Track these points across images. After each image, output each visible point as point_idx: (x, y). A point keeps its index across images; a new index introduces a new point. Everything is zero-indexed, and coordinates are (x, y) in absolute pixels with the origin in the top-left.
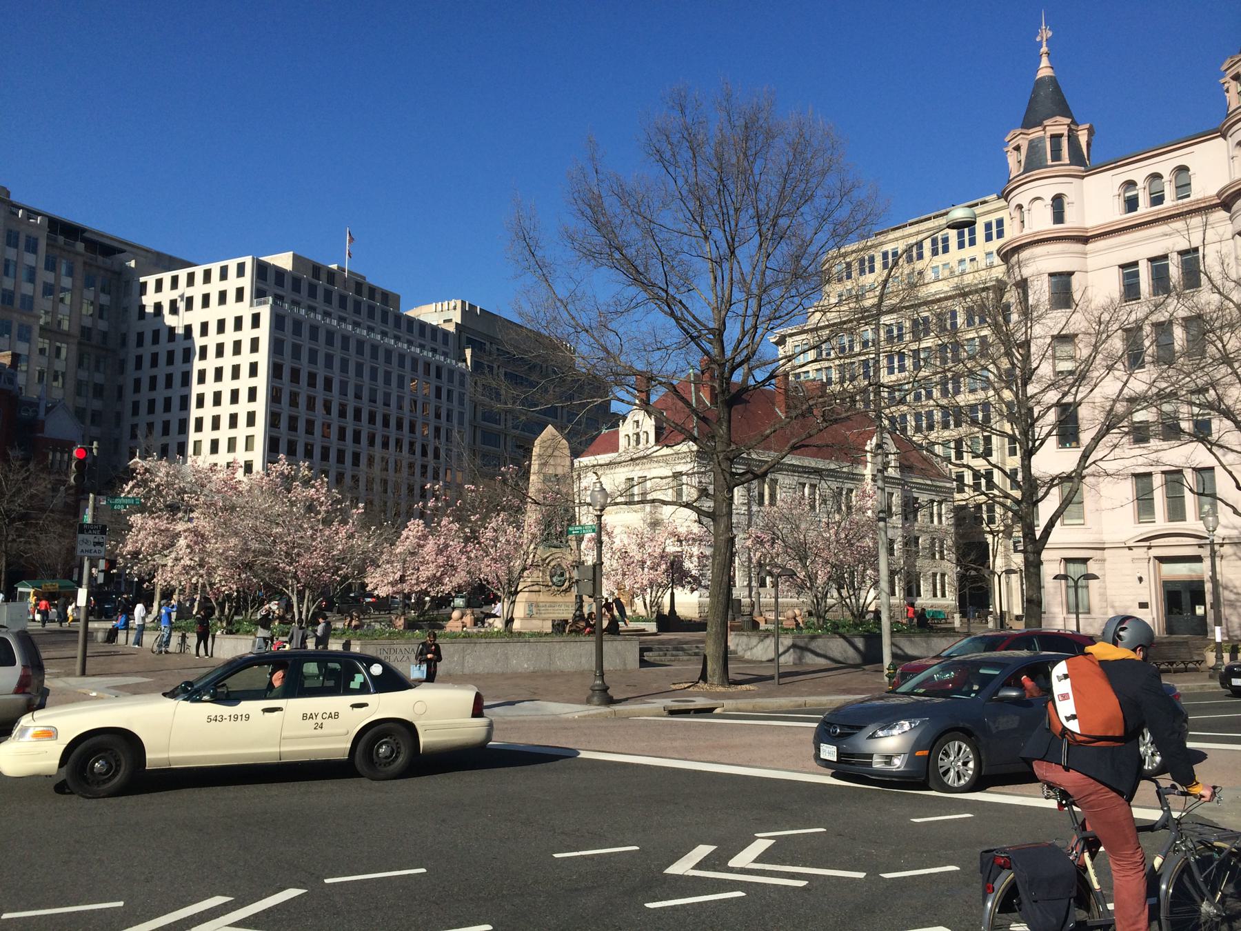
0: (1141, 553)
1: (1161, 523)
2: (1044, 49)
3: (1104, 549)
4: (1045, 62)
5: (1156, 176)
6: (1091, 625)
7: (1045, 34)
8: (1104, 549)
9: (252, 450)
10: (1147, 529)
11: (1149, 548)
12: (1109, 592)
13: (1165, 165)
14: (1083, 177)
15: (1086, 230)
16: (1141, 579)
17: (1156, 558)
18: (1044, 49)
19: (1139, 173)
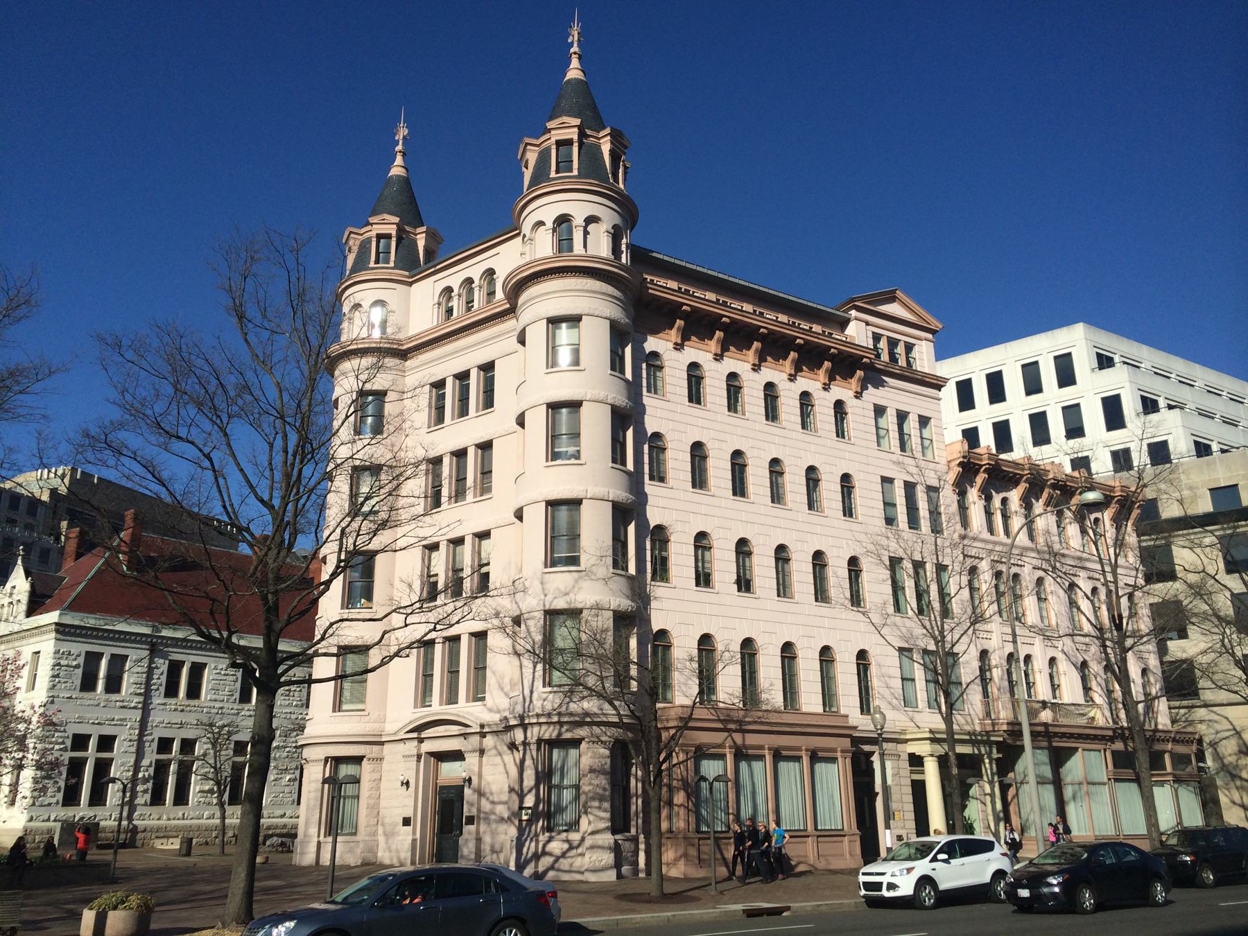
0: (411, 747)
1: (437, 709)
2: (575, 48)
3: (382, 743)
4: (575, 62)
5: (469, 281)
6: (351, 851)
7: (403, 132)
8: (382, 743)
9: (1065, 409)
10: (425, 715)
11: (421, 740)
12: (383, 803)
13: (474, 269)
14: (410, 284)
15: (399, 342)
16: (407, 783)
17: (432, 754)
18: (575, 48)
19: (454, 279)
